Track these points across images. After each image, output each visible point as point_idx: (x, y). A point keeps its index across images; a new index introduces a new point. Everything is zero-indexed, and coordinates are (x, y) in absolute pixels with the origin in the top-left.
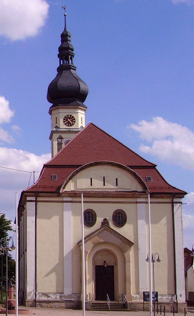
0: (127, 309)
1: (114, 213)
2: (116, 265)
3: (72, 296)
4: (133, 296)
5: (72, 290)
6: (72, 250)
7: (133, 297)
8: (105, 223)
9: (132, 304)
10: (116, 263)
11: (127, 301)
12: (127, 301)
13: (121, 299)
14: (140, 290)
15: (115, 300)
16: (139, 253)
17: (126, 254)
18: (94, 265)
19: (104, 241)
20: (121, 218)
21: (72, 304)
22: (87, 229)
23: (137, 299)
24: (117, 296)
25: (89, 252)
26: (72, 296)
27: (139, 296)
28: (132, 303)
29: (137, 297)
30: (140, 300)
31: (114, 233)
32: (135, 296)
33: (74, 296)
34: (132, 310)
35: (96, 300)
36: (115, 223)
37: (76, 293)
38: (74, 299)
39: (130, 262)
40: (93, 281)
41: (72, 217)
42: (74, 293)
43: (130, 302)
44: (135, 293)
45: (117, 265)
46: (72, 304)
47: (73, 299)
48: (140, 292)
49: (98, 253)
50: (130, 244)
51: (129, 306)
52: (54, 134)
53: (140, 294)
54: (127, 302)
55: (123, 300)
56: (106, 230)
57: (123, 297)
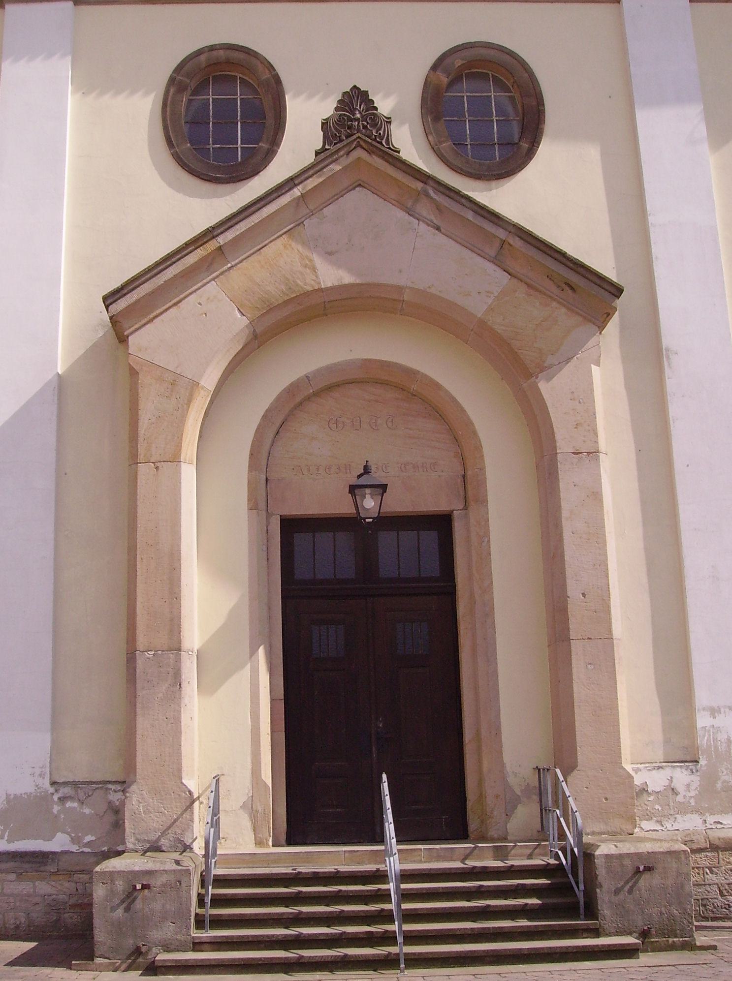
0: (596, 932)
1: (435, 67)
2: (466, 508)
3: (56, 809)
4: (638, 780)
5: (57, 750)
6: (61, 385)
7: (644, 790)
8: (355, 123)
9: (649, 869)
10: (469, 486)
11: (586, 839)
12: (586, 839)
13: (525, 815)
14: (703, 721)
15: (473, 824)
16: (671, 384)
17: (552, 390)
18: (269, 515)
19: (348, 279)
20: (494, 118)
21: (44, 887)
22: (201, 197)
23: (684, 809)
24: (491, 790)
25: (210, 380)
26: (56, 809)
27: (696, 779)
28: (644, 866)
29: (680, 788)
30: (711, 819)
31: (439, 209)
32: (656, 780)
33: (69, 804)
34: (651, 938)
35: (290, 842)
36: (446, 145)
37: (98, 777)
38: (73, 841)
39: (594, 454)
40: (253, 652)
41: (71, 101)
42: (75, 784)
43: (627, 848)
44: (660, 756)
45: (483, 501)
46: (44, 887)
47: (59, 843)
48: (703, 741)
49: (296, 403)
50: (587, 293)
51: (617, 892)
52: (437, 573)
53: (703, 762)
54: (588, 856)
55: (552, 831)
56: (360, 185)
57: (546, 795)
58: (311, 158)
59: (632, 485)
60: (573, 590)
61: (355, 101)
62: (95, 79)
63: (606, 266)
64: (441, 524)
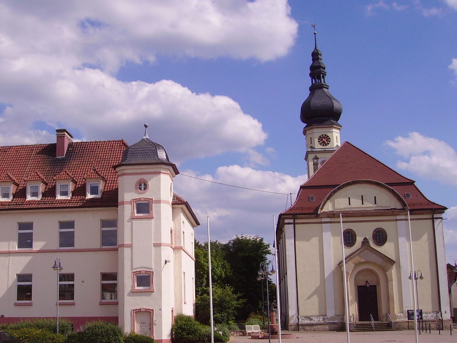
5: (335, 312)
8: (365, 242)
10: (378, 282)
13: (385, 318)
14: (404, 309)
16: (401, 271)
21: (335, 326)
28: (397, 323)
32: (399, 315)
39: (392, 280)
41: (331, 238)
45: (380, 284)
46: (335, 326)
49: (359, 273)
50: (392, 262)
57: (387, 316)
58: (309, 92)
59: (396, 283)
60: (390, 295)
61: (365, 239)
62: (334, 235)
63: (393, 258)
64: (375, 287)
